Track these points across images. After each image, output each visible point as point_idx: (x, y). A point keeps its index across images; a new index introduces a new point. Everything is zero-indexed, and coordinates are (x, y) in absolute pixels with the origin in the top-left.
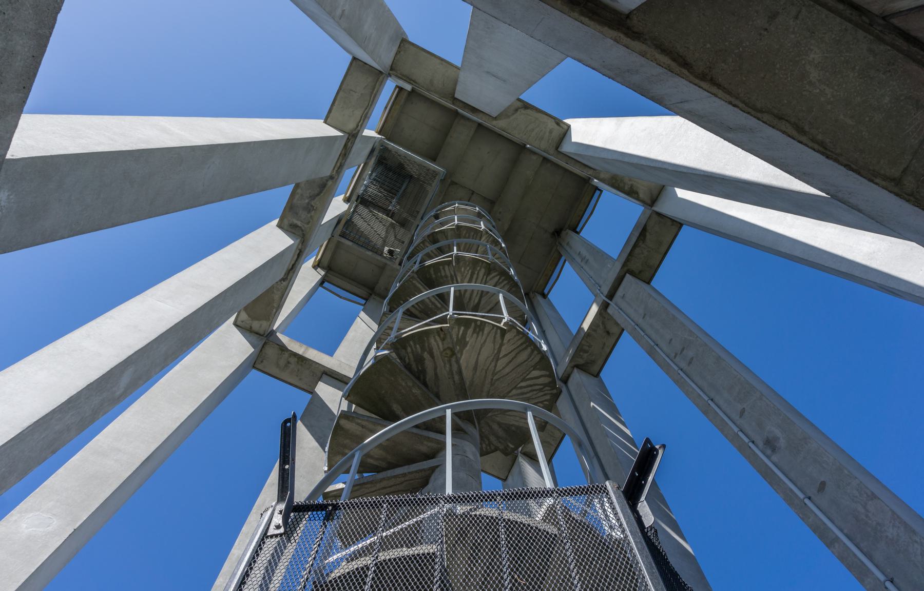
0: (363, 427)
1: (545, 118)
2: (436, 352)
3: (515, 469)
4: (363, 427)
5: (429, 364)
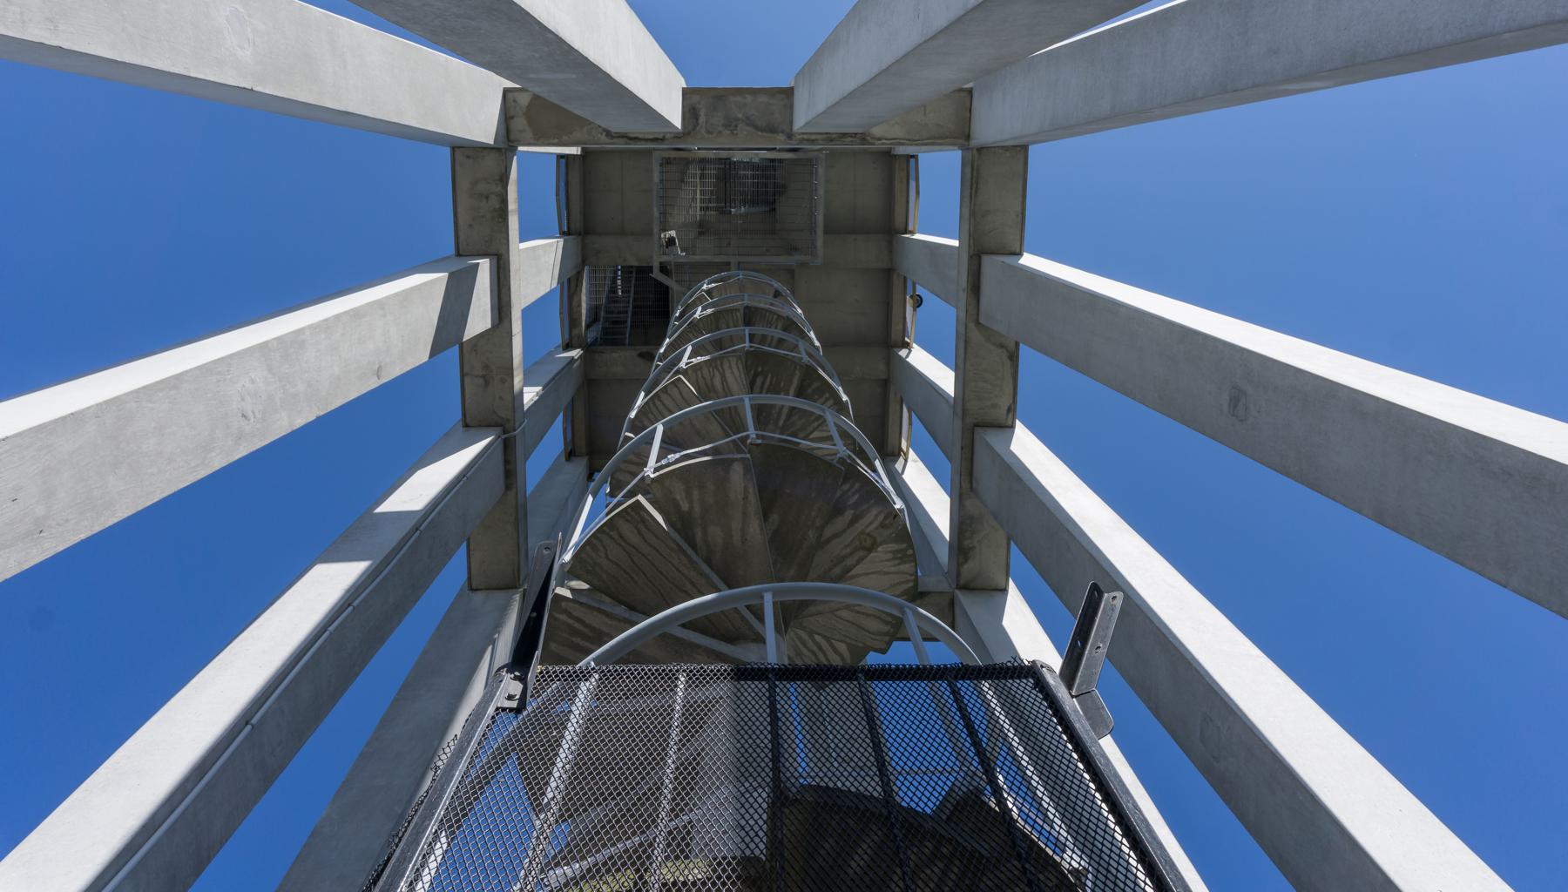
0: (745, 498)
1: (1009, 390)
2: (859, 526)
3: (499, 596)
4: (745, 498)
5: (840, 523)
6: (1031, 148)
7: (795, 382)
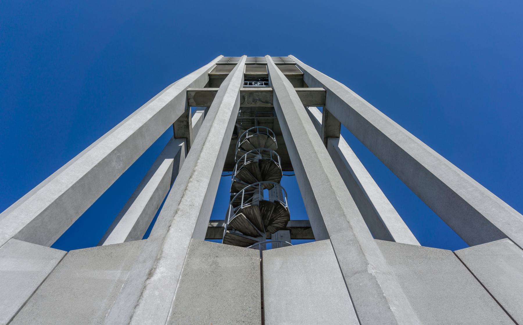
6: (328, 241)
7: (273, 209)
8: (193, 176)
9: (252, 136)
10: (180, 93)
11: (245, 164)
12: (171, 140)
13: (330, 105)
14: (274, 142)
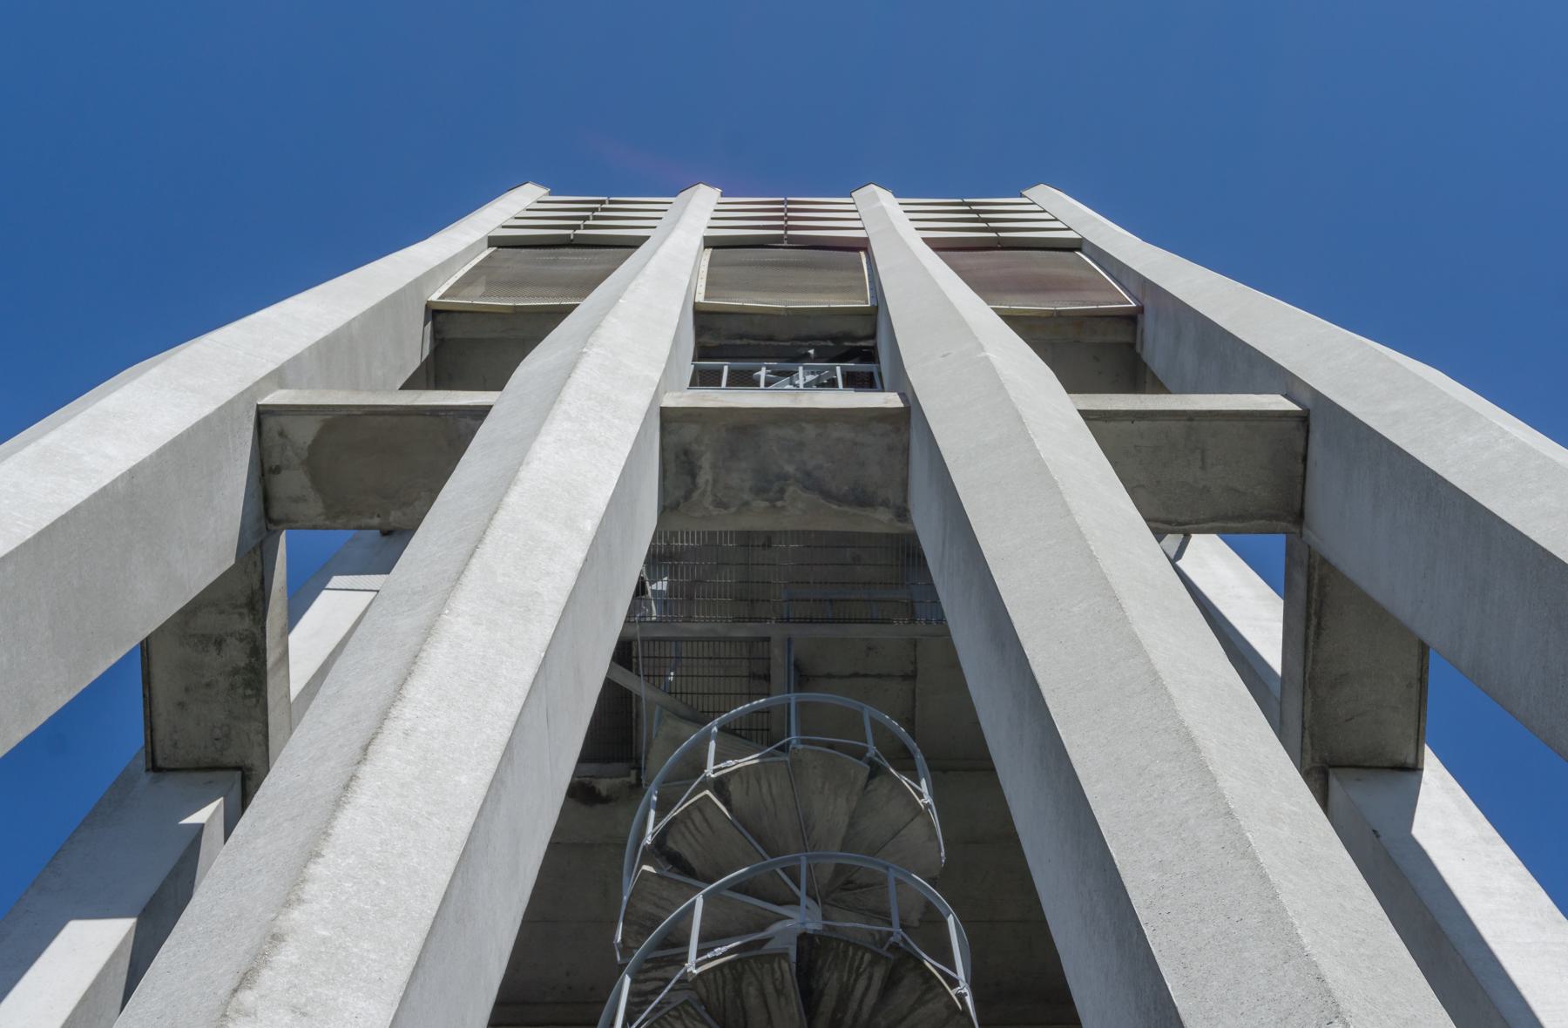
8: (266, 974)
9: (751, 760)
10: (206, 420)
11: (692, 967)
12: (125, 782)
13: (1347, 529)
14: (919, 812)
